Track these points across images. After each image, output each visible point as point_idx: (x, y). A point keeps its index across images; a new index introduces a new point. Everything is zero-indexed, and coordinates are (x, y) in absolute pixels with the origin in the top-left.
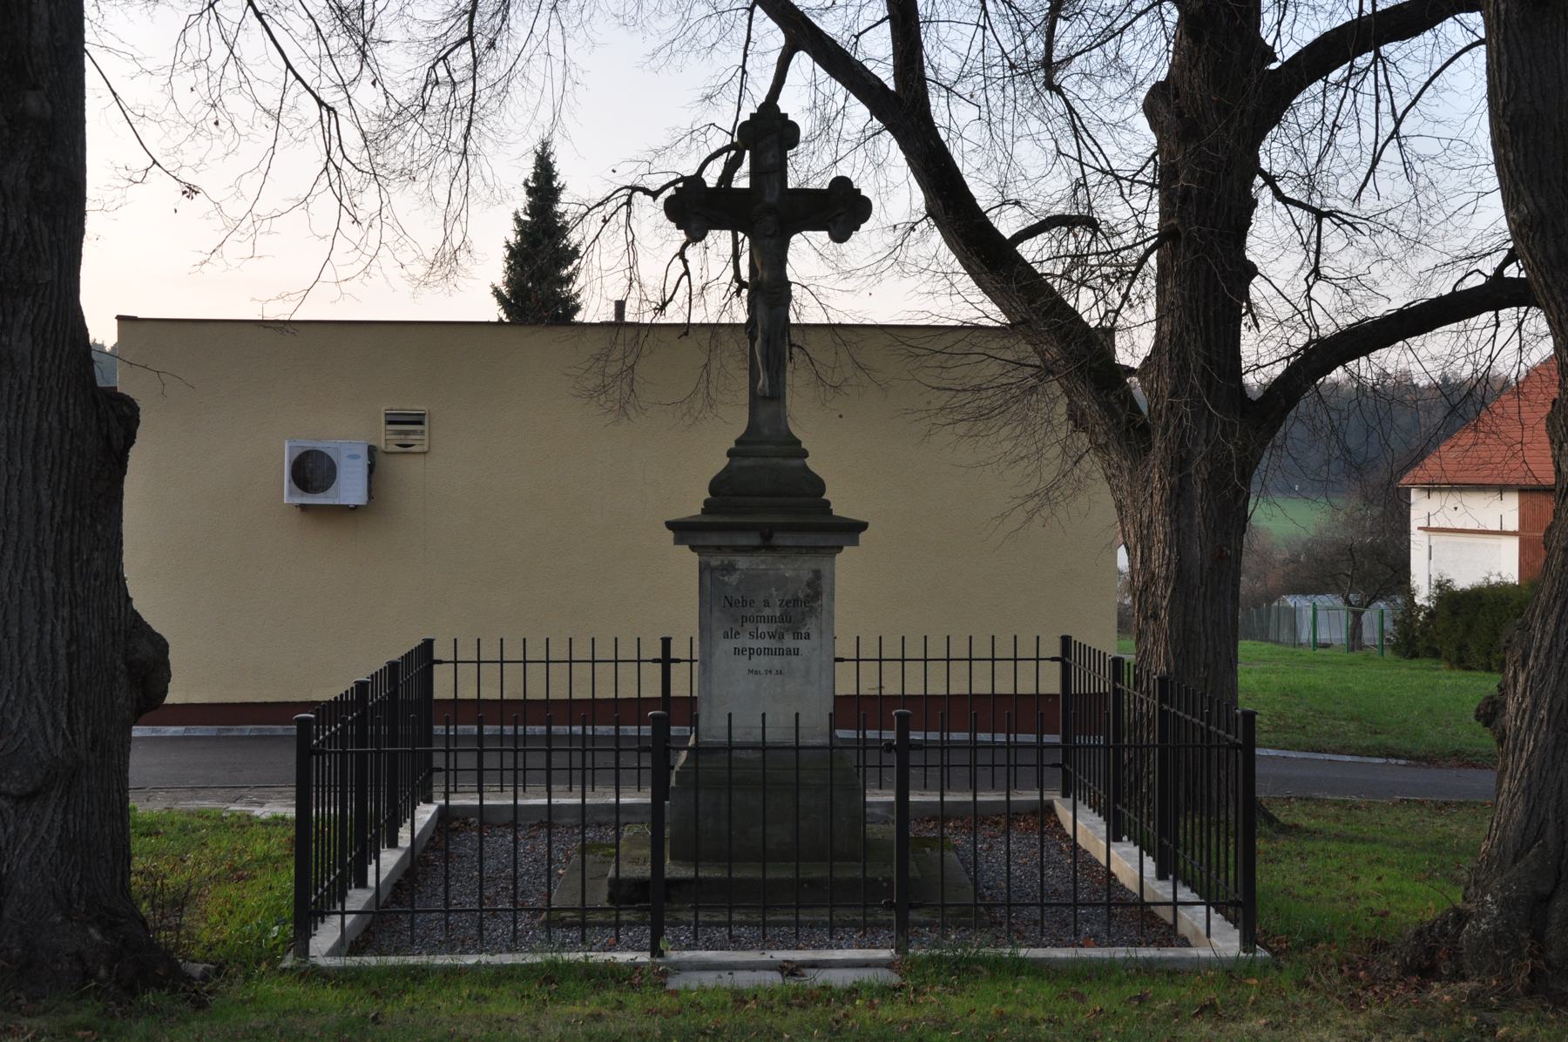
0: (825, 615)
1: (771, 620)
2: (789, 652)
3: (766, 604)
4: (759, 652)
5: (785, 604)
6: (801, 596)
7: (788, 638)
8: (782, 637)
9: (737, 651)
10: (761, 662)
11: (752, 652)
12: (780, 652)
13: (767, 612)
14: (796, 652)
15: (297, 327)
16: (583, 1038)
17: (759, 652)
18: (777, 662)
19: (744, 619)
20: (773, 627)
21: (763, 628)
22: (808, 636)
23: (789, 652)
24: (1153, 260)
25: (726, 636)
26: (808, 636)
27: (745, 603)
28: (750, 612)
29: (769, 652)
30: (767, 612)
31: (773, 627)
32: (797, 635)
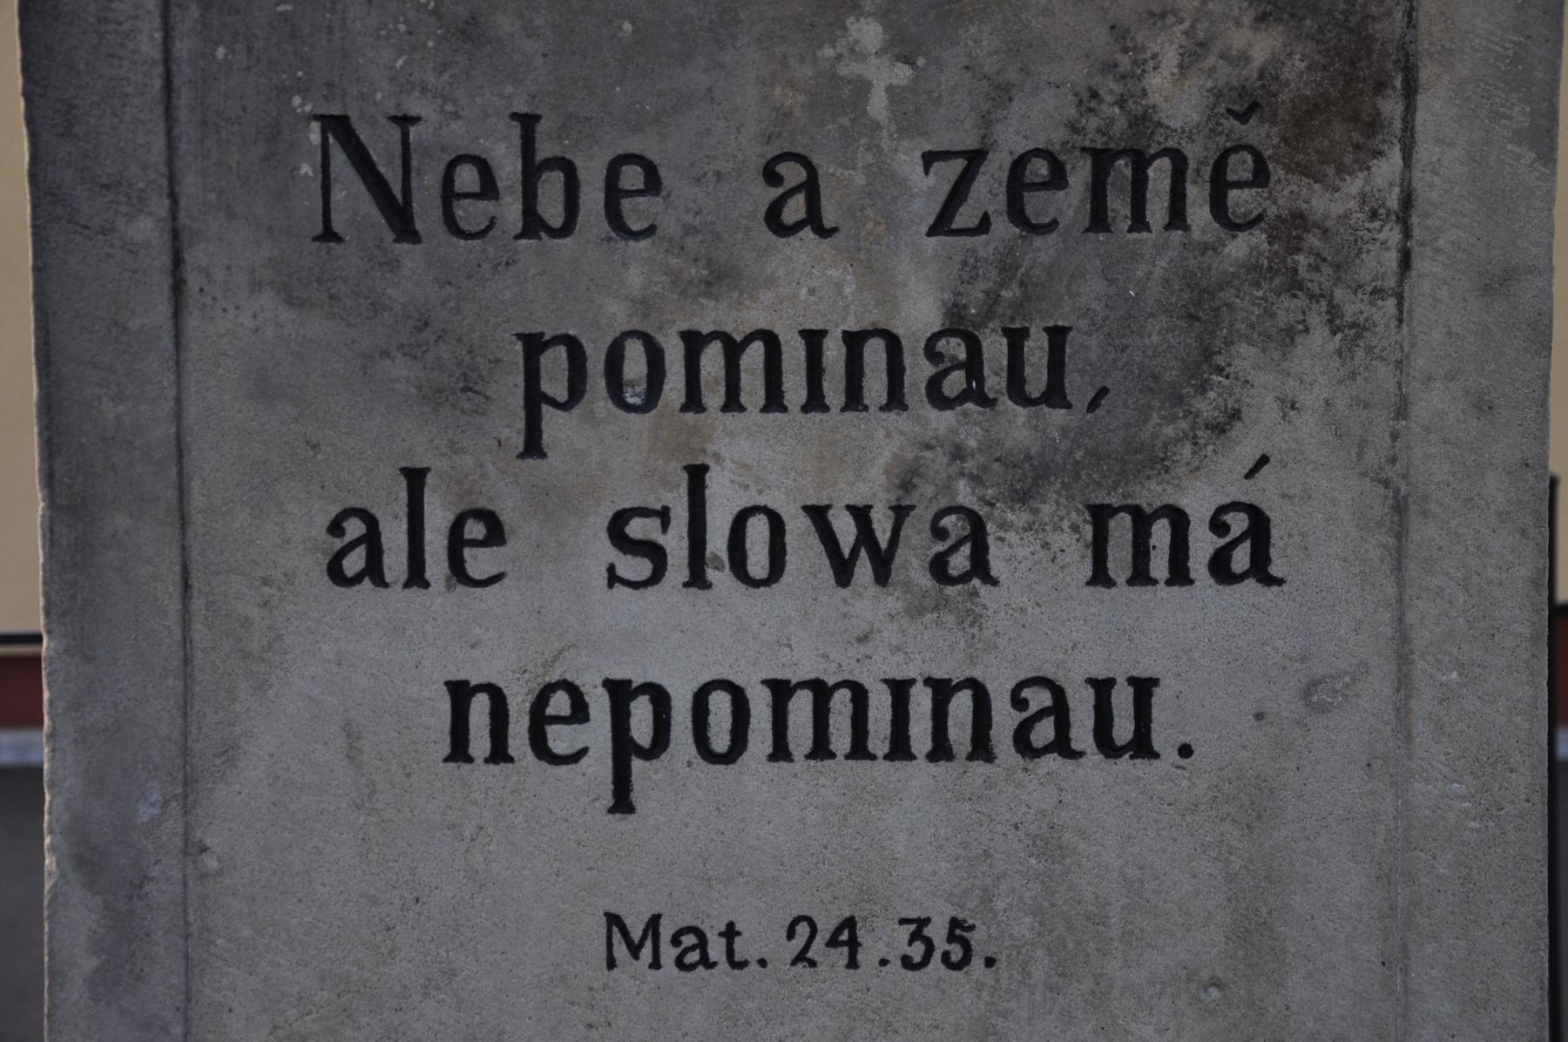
0: (1441, 304)
1: (843, 371)
2: (1047, 723)
3: (796, 200)
4: (725, 723)
5: (998, 191)
6: (1178, 101)
7: (1036, 563)
8: (966, 559)
9: (478, 720)
10: (747, 833)
11: (639, 725)
12: (951, 722)
13: (804, 286)
14: (1126, 720)
15: (1540, 533)
16: (504, 23)
17: (725, 723)
18: (914, 827)
19: (556, 373)
20: (863, 457)
21: (759, 461)
22: (1250, 548)
23: (1047, 723)
24: (331, 140)
25: (355, 556)
26: (1250, 548)
27: (548, 190)
28: (605, 288)
29: (825, 718)
30: (804, 286)
31: (863, 457)
32: (1132, 542)
